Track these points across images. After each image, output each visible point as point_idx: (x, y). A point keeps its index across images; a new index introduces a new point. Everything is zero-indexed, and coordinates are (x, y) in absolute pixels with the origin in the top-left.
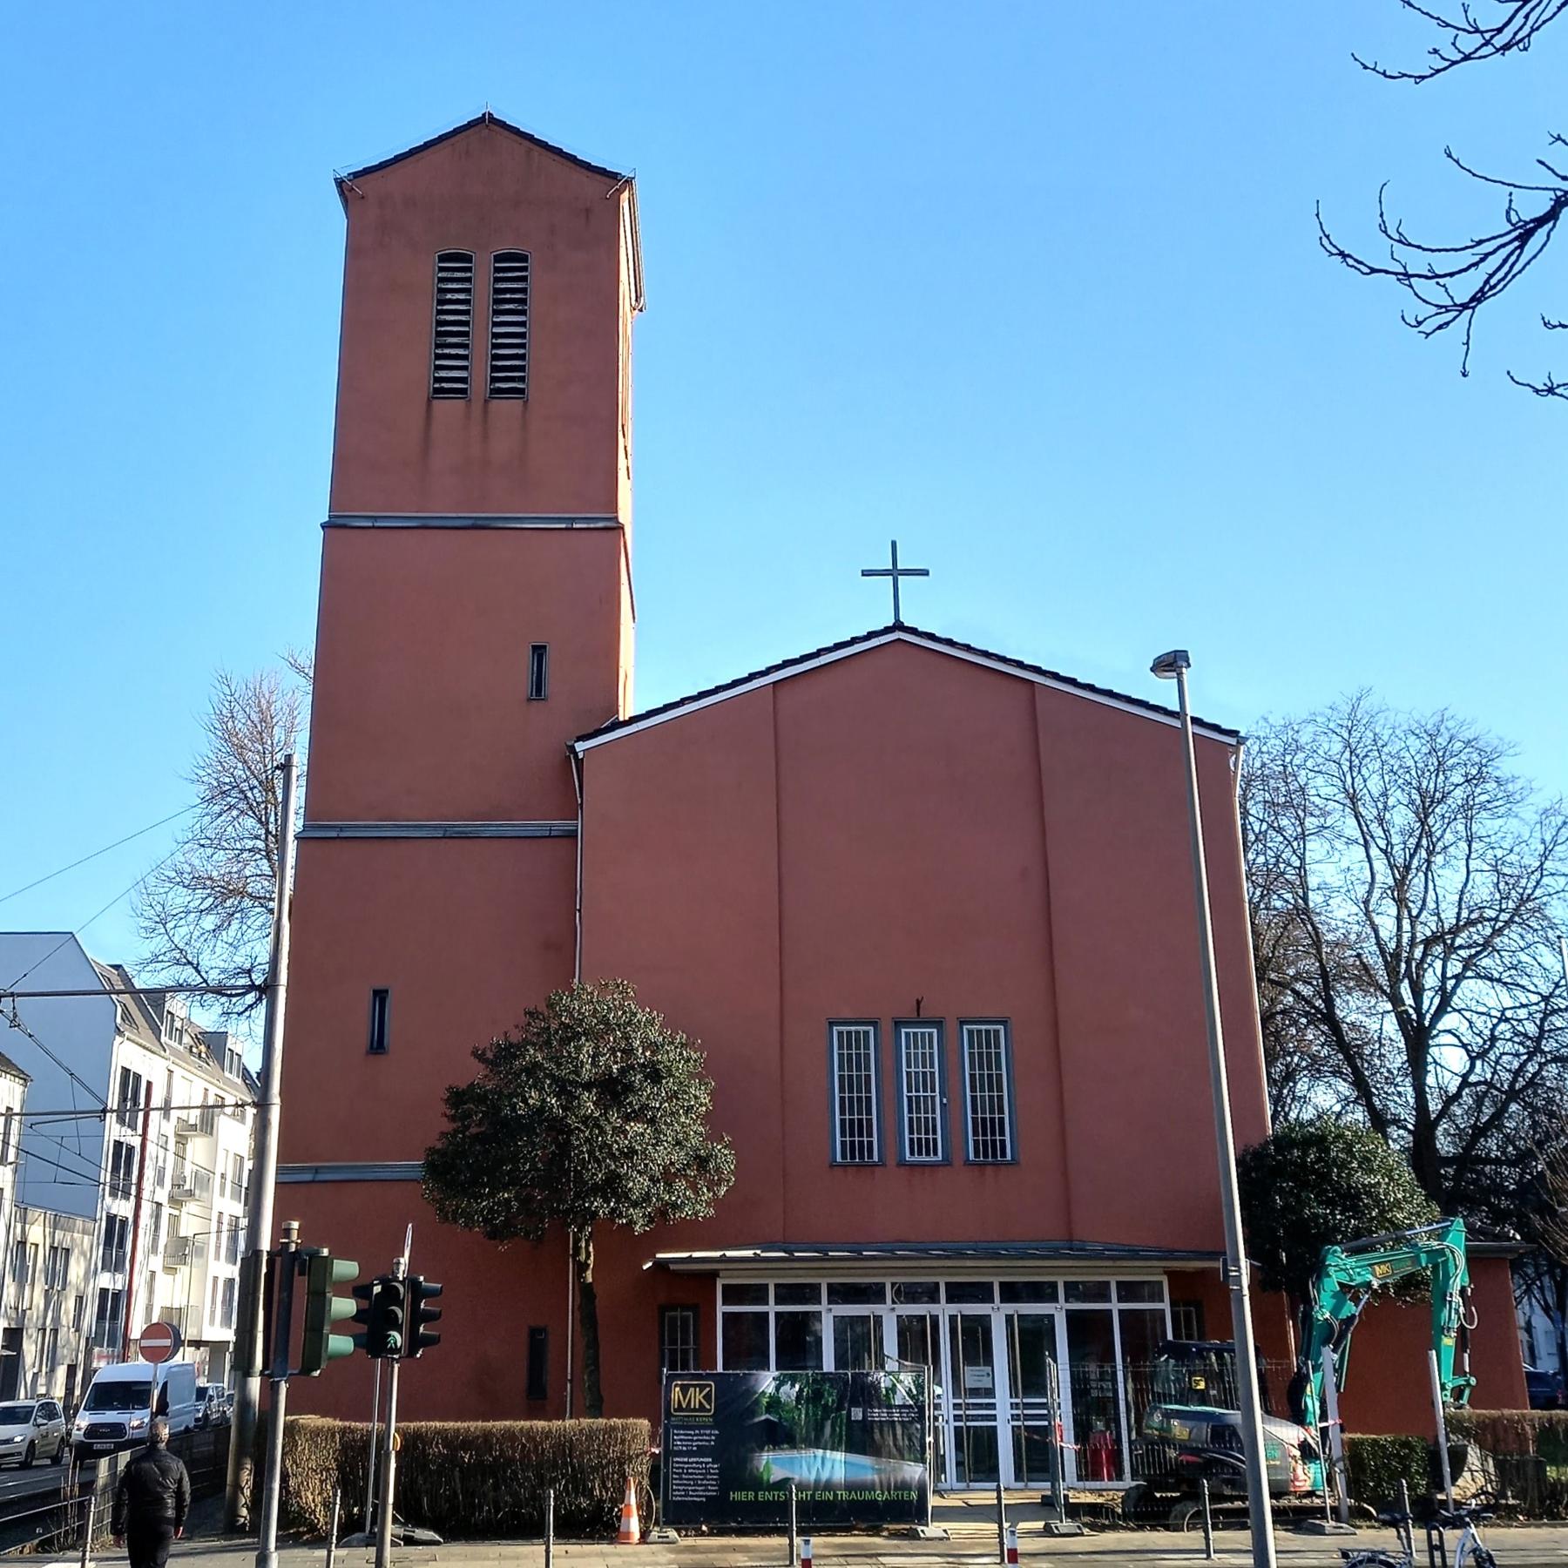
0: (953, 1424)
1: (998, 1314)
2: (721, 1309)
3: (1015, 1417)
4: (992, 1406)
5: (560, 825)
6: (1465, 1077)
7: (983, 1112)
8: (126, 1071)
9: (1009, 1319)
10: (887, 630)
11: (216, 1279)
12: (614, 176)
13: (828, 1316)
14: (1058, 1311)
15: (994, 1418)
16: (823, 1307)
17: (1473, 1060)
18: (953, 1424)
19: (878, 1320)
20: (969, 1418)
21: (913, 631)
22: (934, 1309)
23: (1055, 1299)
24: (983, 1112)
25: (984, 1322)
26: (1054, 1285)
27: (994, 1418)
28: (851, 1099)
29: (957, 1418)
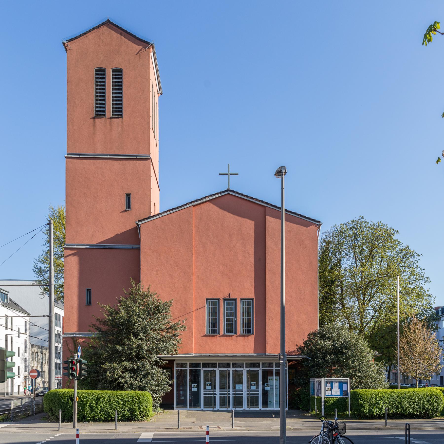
0: (232, 395)
1: (245, 370)
2: (175, 368)
3: (248, 394)
4: (215, 391)
5: (136, 246)
6: (373, 316)
7: (246, 322)
8: (56, 314)
9: (248, 371)
10: (226, 191)
11: (19, 356)
12: (148, 43)
13: (202, 370)
14: (260, 370)
15: (258, 394)
16: (201, 368)
17: (375, 312)
18: (232, 395)
19: (215, 371)
20: (237, 394)
21: (232, 191)
22: (229, 369)
23: (259, 367)
24: (246, 322)
25: (257, 373)
26: (259, 364)
27: (243, 394)
28: (212, 318)
29: (233, 394)
